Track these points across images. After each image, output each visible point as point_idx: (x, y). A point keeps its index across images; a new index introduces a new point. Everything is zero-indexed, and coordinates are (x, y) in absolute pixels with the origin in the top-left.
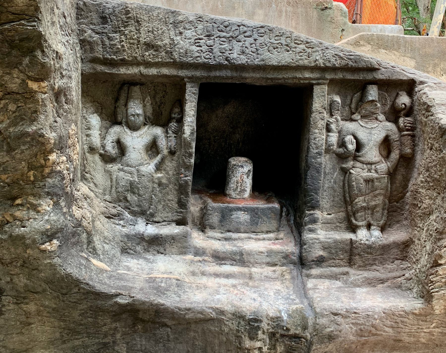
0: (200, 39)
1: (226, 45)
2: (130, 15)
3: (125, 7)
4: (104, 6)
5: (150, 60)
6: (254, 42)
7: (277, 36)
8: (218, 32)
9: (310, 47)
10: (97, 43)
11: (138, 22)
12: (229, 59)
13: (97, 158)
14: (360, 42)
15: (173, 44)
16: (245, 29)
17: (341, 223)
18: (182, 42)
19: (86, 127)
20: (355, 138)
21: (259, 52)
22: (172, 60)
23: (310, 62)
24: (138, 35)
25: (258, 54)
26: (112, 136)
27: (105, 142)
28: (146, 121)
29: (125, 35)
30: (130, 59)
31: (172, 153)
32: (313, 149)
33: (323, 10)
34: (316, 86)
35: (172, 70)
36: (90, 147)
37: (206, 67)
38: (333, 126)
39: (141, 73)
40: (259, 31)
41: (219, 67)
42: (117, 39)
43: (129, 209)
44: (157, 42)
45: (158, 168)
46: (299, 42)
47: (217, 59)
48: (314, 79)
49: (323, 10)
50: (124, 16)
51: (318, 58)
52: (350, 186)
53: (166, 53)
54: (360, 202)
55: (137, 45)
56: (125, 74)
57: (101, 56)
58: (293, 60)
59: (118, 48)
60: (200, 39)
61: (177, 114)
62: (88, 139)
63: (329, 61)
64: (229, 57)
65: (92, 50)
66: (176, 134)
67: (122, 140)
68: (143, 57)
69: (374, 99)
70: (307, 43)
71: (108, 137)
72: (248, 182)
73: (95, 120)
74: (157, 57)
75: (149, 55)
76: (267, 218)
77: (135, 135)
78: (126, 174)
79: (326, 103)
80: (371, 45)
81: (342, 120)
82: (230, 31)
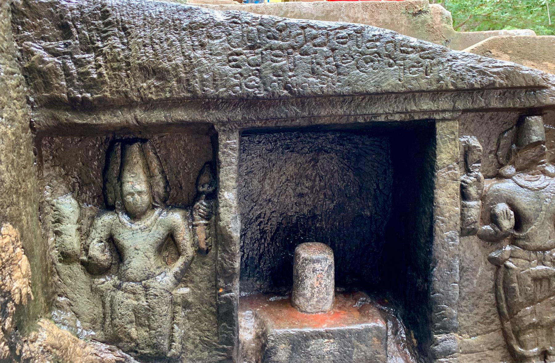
0: (238, 54)
1: (284, 62)
2: (110, 19)
3: (100, 5)
4: (63, 6)
5: (150, 95)
6: (331, 54)
7: (370, 41)
8: (268, 40)
9: (428, 58)
10: (55, 73)
11: (124, 29)
12: (289, 85)
13: (77, 268)
14: (491, 51)
15: (190, 65)
16: (314, 32)
17: (492, 350)
18: (204, 61)
19: (53, 220)
20: (512, 206)
21: (340, 70)
22: (189, 95)
23: (431, 84)
24: (127, 52)
25: (339, 74)
26: (99, 231)
27: (88, 241)
28: (156, 202)
29: (104, 55)
30: (116, 97)
31: (201, 252)
32: (442, 231)
33: (415, 15)
34: (440, 123)
35: (190, 111)
36: (62, 253)
37: (249, 102)
38: (472, 191)
39: (136, 120)
40: (339, 35)
41: (272, 101)
42: (89, 62)
43: (136, 352)
44: (161, 63)
45: (181, 279)
46: (410, 49)
47: (269, 88)
48: (437, 112)
49: (415, 15)
50: (100, 22)
51: (443, 75)
52: (508, 290)
53: (179, 81)
54: (528, 315)
55: (126, 70)
56: (110, 124)
57: (65, 95)
58: (400, 80)
59: (93, 79)
60: (238, 54)
61: (207, 186)
62: (59, 239)
63: (463, 79)
64: (289, 83)
65: (48, 86)
66: (208, 219)
67: (116, 237)
68: (139, 91)
69: (541, 139)
70: (423, 50)
71: (93, 233)
72: (329, 282)
73: (68, 205)
74: (163, 90)
75: (149, 88)
76: (366, 346)
77: (137, 227)
78: (126, 294)
79: (458, 152)
80: (509, 54)
81: (486, 177)
82: (289, 36)
